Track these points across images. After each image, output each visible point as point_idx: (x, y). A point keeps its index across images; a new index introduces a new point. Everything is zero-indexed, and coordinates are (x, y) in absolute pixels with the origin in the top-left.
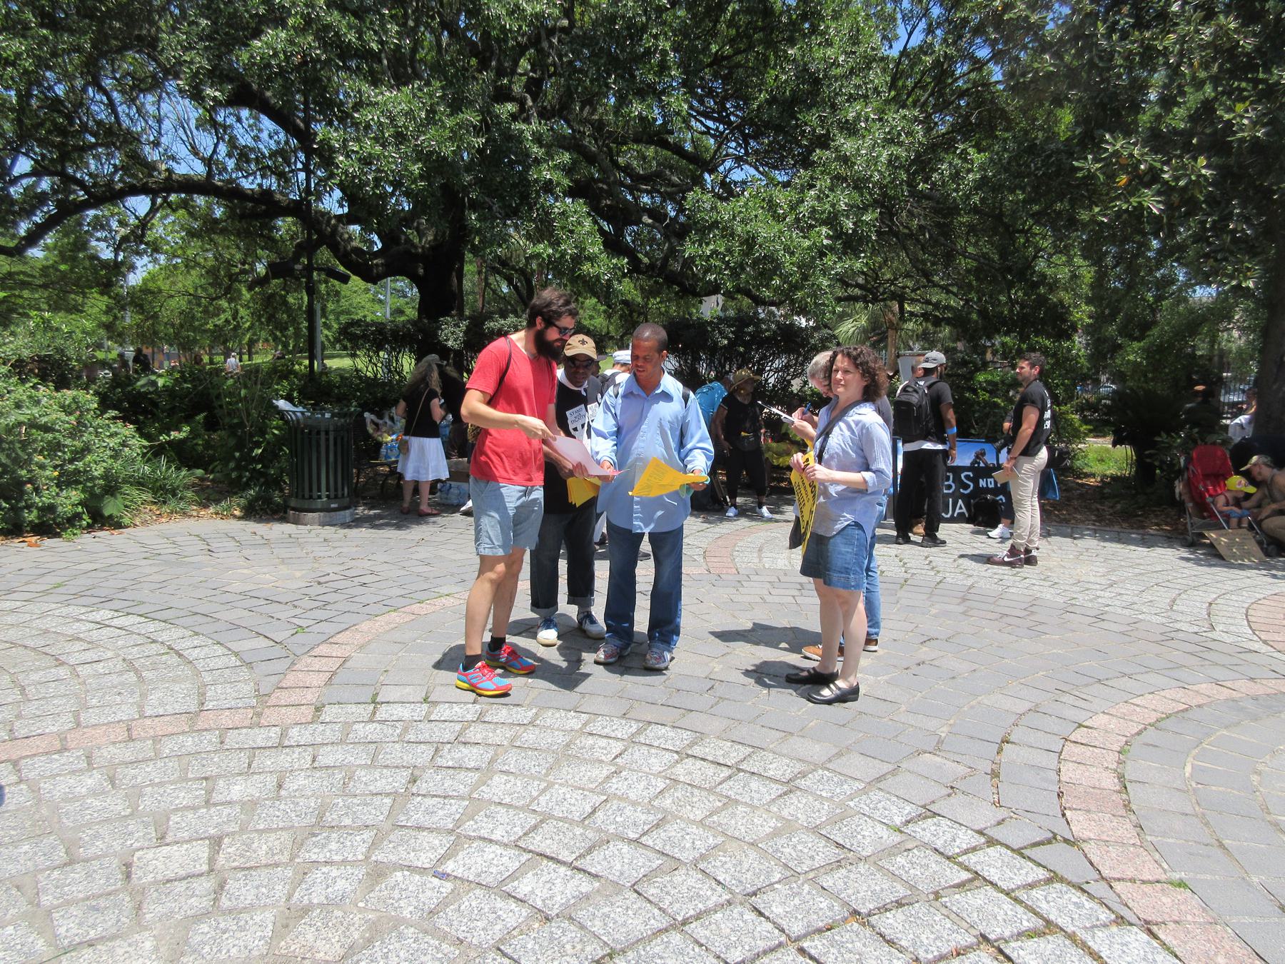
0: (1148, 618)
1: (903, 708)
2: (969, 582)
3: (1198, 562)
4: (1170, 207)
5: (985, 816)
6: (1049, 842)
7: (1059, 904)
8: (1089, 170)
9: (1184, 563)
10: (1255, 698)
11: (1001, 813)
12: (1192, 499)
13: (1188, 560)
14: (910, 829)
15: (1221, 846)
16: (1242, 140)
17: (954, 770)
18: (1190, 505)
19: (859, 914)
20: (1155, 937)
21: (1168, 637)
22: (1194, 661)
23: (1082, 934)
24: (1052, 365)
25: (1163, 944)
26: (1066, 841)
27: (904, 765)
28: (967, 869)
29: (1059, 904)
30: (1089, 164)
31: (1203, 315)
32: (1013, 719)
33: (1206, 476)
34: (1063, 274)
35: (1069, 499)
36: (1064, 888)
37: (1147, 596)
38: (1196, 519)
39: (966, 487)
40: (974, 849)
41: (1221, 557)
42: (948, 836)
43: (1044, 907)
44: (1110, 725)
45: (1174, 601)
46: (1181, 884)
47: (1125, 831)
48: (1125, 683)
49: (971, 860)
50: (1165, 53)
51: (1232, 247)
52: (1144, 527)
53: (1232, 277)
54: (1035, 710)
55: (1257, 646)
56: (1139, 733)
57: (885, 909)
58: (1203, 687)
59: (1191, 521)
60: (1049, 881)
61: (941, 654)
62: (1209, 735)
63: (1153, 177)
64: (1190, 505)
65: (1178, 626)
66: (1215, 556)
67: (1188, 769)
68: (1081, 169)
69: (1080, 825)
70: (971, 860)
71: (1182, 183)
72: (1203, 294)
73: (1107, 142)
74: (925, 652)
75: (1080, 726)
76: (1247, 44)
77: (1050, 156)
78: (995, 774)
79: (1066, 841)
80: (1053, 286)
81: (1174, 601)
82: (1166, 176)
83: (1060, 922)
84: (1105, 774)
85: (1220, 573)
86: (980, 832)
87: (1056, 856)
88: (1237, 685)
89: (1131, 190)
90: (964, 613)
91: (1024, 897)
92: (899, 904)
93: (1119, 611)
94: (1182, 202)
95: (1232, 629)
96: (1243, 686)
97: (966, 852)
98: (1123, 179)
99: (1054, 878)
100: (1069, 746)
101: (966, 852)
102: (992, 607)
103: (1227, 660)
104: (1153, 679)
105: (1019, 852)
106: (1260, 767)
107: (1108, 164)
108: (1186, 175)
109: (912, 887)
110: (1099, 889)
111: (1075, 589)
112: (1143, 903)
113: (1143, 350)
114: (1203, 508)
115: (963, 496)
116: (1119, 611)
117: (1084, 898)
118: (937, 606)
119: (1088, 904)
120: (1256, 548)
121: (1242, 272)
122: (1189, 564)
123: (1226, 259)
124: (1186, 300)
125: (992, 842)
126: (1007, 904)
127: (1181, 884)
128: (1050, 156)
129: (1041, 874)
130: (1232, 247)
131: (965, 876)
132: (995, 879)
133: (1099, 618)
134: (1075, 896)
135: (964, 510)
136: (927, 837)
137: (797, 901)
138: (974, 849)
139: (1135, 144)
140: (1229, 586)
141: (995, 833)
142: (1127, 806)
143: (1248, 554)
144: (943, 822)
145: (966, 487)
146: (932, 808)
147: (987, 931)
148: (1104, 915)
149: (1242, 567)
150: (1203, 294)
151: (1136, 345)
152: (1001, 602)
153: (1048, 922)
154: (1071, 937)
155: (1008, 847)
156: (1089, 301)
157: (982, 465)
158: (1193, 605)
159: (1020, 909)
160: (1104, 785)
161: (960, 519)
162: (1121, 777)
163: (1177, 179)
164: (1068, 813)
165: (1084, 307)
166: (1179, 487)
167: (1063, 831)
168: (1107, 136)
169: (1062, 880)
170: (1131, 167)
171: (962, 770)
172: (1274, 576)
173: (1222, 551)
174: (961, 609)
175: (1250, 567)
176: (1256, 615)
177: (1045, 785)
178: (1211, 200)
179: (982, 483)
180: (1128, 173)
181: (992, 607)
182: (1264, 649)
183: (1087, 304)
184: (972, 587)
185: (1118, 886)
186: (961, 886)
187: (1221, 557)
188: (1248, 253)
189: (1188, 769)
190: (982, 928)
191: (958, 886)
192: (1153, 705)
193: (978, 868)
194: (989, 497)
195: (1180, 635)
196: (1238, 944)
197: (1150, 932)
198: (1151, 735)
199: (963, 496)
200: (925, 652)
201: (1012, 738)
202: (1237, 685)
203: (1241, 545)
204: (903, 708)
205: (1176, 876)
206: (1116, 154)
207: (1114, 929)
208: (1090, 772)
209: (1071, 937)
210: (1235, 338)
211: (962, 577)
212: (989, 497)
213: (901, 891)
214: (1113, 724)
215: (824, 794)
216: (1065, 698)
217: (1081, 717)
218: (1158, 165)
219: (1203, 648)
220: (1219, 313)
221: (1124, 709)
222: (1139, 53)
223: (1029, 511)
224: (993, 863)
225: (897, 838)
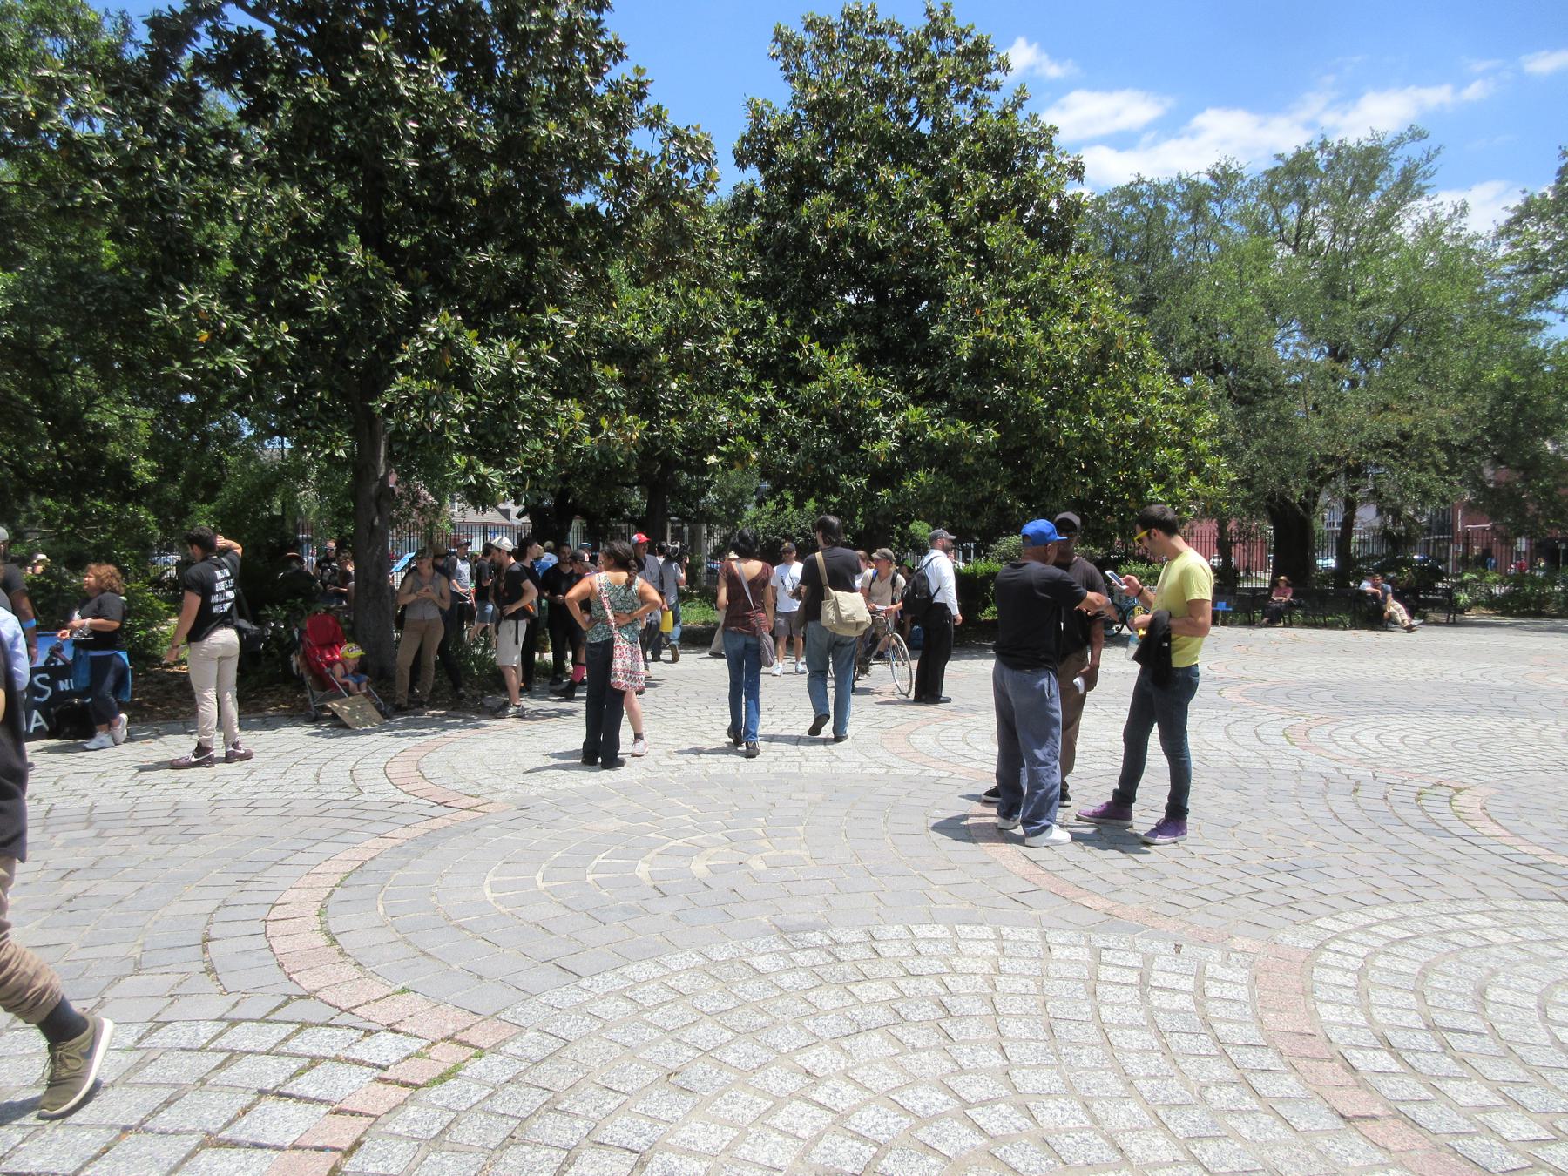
0: (299, 796)
1: (75, 946)
2: (88, 802)
3: (326, 735)
4: (257, 369)
5: (220, 1005)
6: (286, 1003)
7: (314, 1042)
8: (165, 321)
9: (314, 739)
10: (414, 840)
11: (233, 999)
12: (311, 671)
13: (316, 735)
14: (146, 1043)
15: (425, 954)
16: (320, 313)
17: (163, 983)
18: (309, 679)
19: (130, 1128)
20: (397, 1032)
21: (323, 810)
22: (352, 824)
23: (344, 1054)
24: (114, 534)
25: (406, 1034)
26: (301, 997)
27: (108, 995)
28: (222, 1051)
29: (314, 1042)
30: (161, 314)
31: (275, 474)
32: (205, 919)
33: (322, 646)
34: (112, 422)
35: (167, 692)
36: (315, 1029)
37: (290, 777)
38: (316, 693)
39: (41, 693)
40: (221, 1034)
41: (346, 726)
42: (190, 1034)
43: (304, 1049)
44: (300, 894)
45: (318, 775)
46: (405, 990)
47: (349, 971)
48: (299, 857)
49: (223, 1042)
50: (233, 209)
51: (322, 416)
52: (261, 710)
53: (324, 446)
54: (224, 904)
55: (402, 798)
56: (330, 895)
57: (156, 1112)
58: (371, 843)
59: (312, 695)
60: (299, 1031)
61: (93, 883)
62: (388, 879)
63: (235, 338)
64: (309, 679)
65: (329, 797)
66: (340, 726)
67: (381, 909)
68: (156, 318)
69: (308, 982)
70: (223, 1042)
71: (267, 347)
72: (276, 449)
73: (182, 293)
74: (70, 887)
75: (274, 905)
76: (313, 217)
77: (103, 290)
78: (210, 970)
79: (301, 997)
80: (105, 436)
81: (318, 775)
82: (249, 337)
83: (322, 1053)
84: (314, 936)
85: (347, 743)
86: (220, 1019)
87: (297, 1010)
88: (397, 833)
89: (211, 350)
90: (98, 836)
91: (284, 1049)
92: (168, 1103)
93: (269, 796)
94: (263, 363)
95: (378, 790)
96: (402, 833)
97: (214, 1039)
98: (204, 335)
99: (304, 1025)
100: (271, 925)
101: (214, 1039)
102: (129, 823)
103: (383, 816)
104: (321, 847)
105: (264, 1020)
106: (435, 890)
107: (185, 318)
108: (270, 339)
109: (174, 1085)
110: (345, 1019)
111: (213, 784)
112: (381, 1014)
113: (214, 512)
114: (324, 683)
115: (38, 706)
116: (269, 796)
117: (334, 1030)
118: (60, 836)
119: (339, 1033)
120: (375, 713)
121: (330, 441)
122: (319, 739)
123: (316, 427)
124: (256, 457)
125: (234, 1023)
126: (271, 1060)
127: (405, 990)
128: (103, 290)
129: (291, 1028)
130: (322, 416)
131: (222, 1057)
132: (252, 1047)
133: (251, 806)
134: (326, 1031)
135: (43, 723)
136: (168, 1042)
137: (55, 1146)
138: (221, 1034)
139: (213, 299)
140: (362, 752)
141: (235, 1014)
142: (342, 952)
143: (370, 720)
144: (178, 1025)
145: (41, 693)
146: (159, 1019)
147: (263, 1086)
148: (355, 1035)
149: (367, 732)
150: (276, 449)
151: (206, 508)
152: (136, 815)
153: (313, 1058)
154: (337, 1059)
155: (252, 1020)
156: (147, 455)
157: (60, 663)
158: (336, 775)
159: (285, 1059)
160: (315, 944)
161: (39, 734)
162: (328, 933)
163: (261, 342)
164: (294, 976)
165: (143, 462)
166: (295, 661)
167: (291, 989)
168: (182, 288)
169: (311, 1025)
170: (210, 323)
171: (177, 978)
172: (397, 735)
173: (347, 720)
174: (92, 832)
175: (374, 731)
176: (394, 771)
177: (263, 963)
178: (294, 364)
179: (63, 686)
180: (208, 329)
181: (129, 823)
182: (409, 798)
183: (146, 457)
184: (93, 807)
185: (358, 1011)
186: (221, 1066)
187: (346, 726)
188: (337, 422)
189: (381, 909)
190: (258, 1085)
191: (220, 1067)
192: (345, 860)
193: (232, 1046)
194: (76, 701)
195: (334, 804)
196: (458, 1012)
197: (393, 1031)
198: (340, 894)
199: (38, 706)
200: (70, 887)
201: (213, 935)
202: (397, 833)
203: (362, 711)
204: (75, 946)
205: (399, 987)
206: (194, 307)
207: (367, 1040)
208: (300, 938)
209: (337, 1059)
210: (308, 497)
211: (74, 799)
212: (76, 701)
213: (166, 1093)
214: (304, 894)
215: (27, 1051)
216: (249, 886)
217: (272, 898)
218: (239, 324)
219: (360, 812)
220: (292, 472)
221: (309, 880)
222: (206, 204)
223: (215, 699)
224: (242, 1037)
225: (137, 1055)
